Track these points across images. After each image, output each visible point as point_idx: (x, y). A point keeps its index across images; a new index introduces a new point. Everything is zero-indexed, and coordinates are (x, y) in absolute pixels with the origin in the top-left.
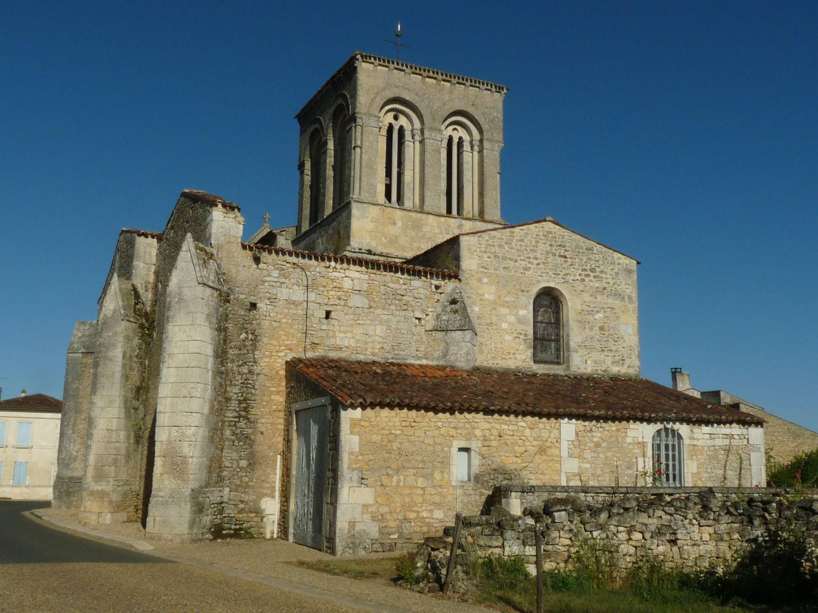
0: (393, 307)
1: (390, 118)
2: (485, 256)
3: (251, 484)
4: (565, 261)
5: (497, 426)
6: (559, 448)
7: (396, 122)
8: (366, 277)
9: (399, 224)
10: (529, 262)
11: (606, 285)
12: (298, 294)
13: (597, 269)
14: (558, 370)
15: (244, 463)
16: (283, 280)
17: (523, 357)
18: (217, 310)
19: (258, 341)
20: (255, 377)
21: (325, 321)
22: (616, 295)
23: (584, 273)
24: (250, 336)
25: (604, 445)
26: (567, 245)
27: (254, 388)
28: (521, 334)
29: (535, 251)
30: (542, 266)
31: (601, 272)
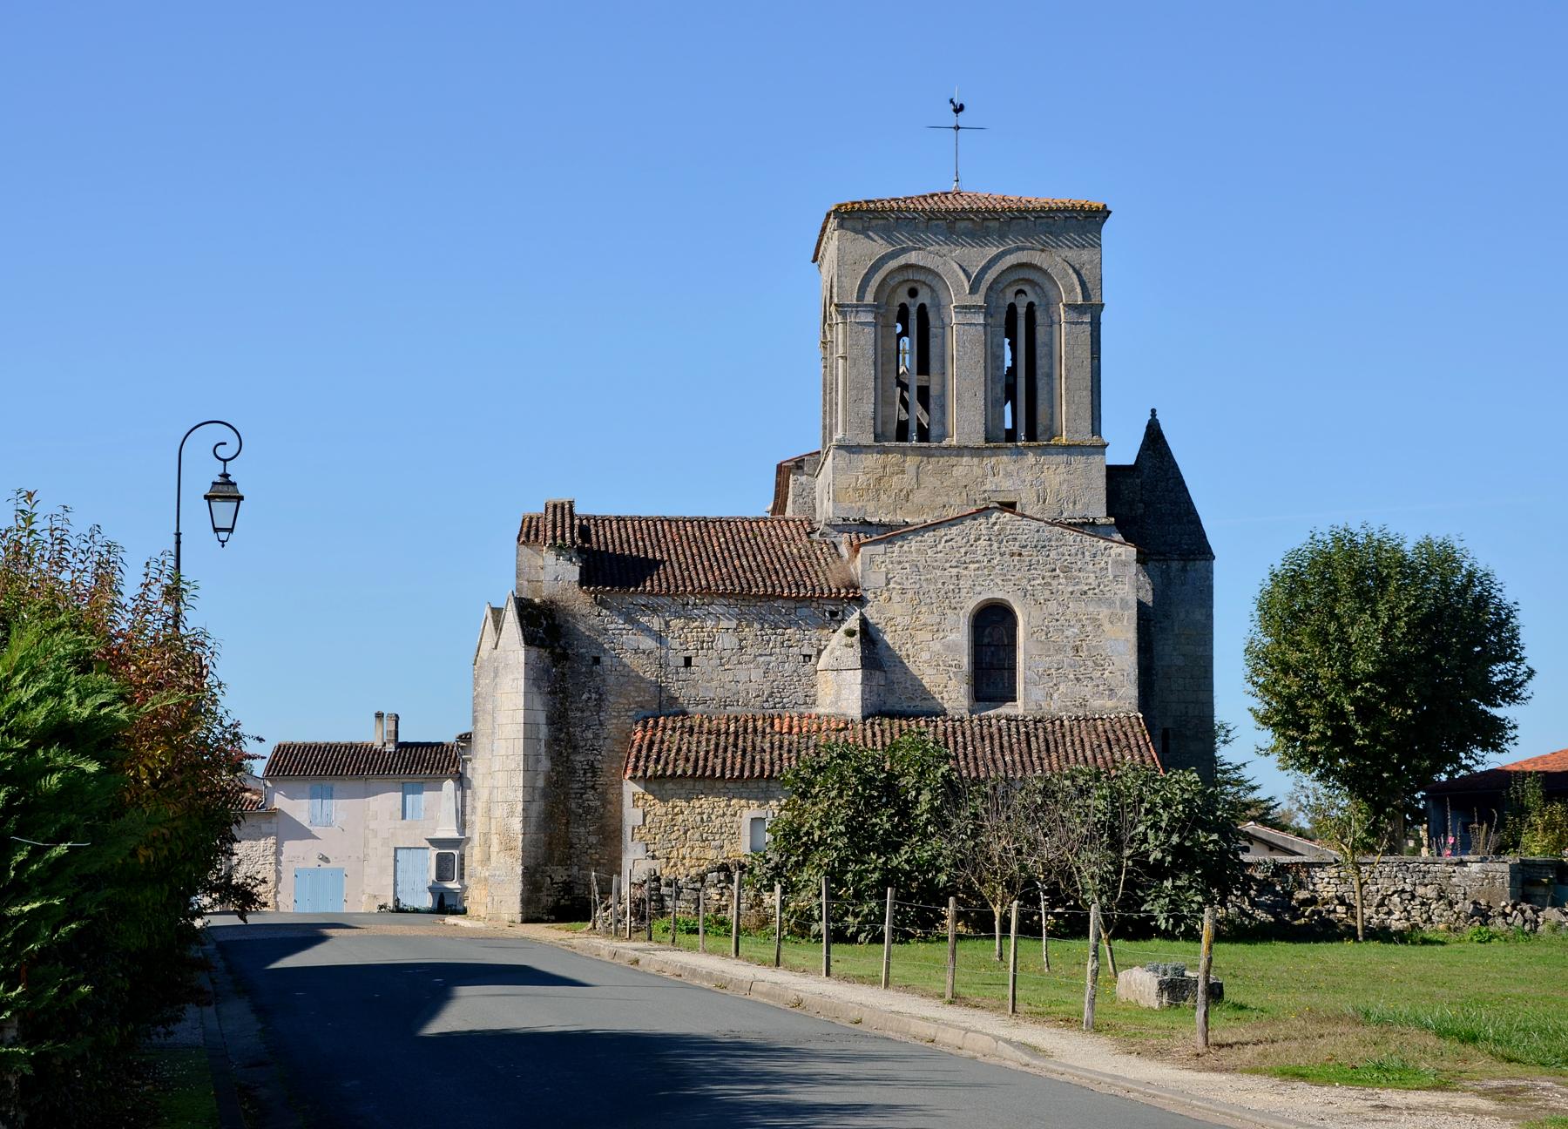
3: (602, 861)
7: (913, 300)
19: (603, 701)
20: (601, 742)
24: (594, 696)
27: (600, 754)
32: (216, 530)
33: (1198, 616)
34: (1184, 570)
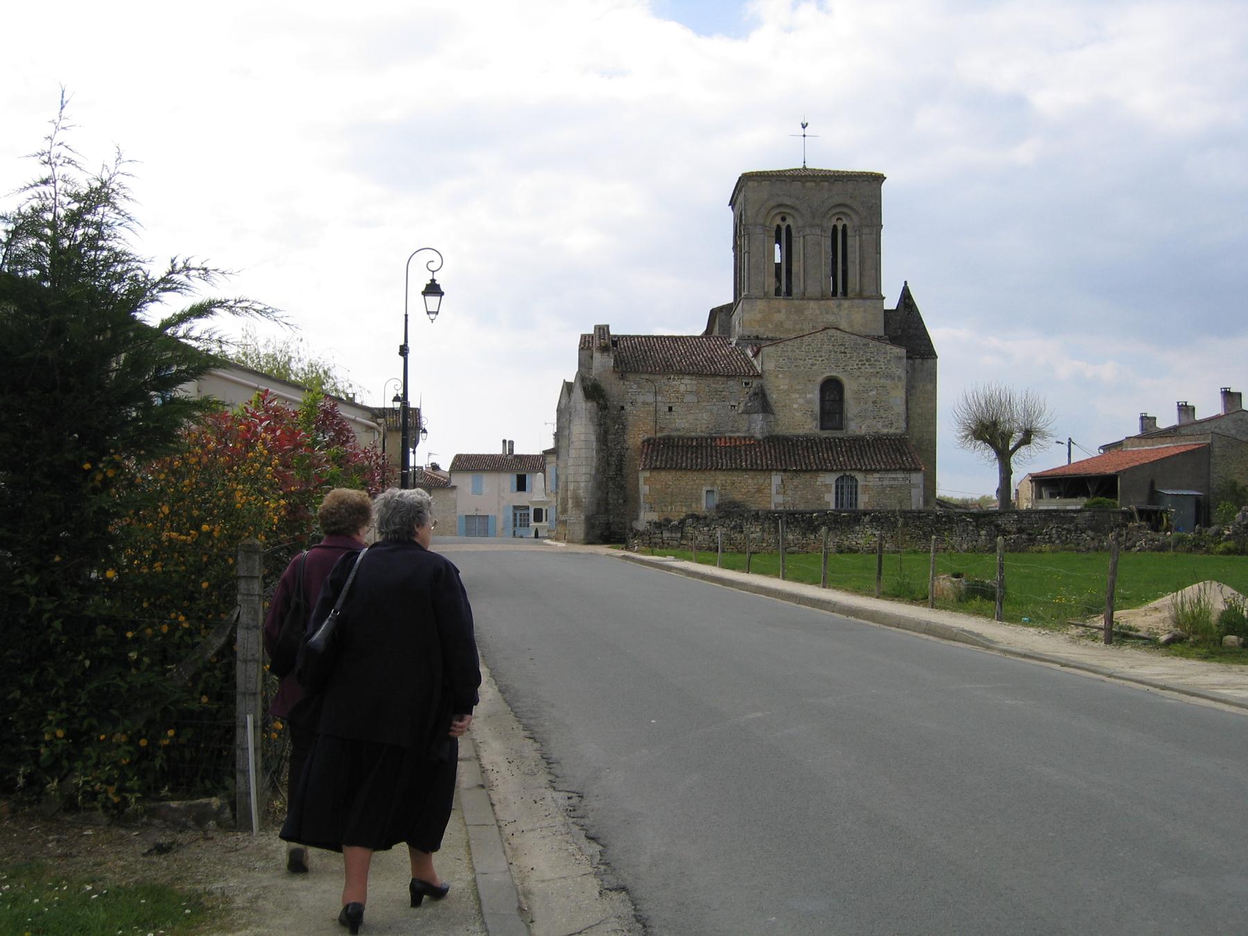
0: (715, 400)
1: (778, 221)
2: (781, 359)
4: (844, 356)
5: (731, 478)
6: (771, 490)
8: (696, 382)
9: (784, 311)
10: (816, 360)
11: (880, 370)
12: (650, 398)
13: (872, 359)
14: (838, 434)
15: (621, 501)
16: (639, 390)
17: (810, 426)
18: (597, 414)
21: (668, 413)
22: (887, 376)
23: (860, 363)
25: (800, 486)
26: (847, 344)
28: (808, 411)
29: (820, 351)
30: (825, 361)
31: (875, 361)
32: (428, 313)
33: (929, 387)
34: (922, 364)
